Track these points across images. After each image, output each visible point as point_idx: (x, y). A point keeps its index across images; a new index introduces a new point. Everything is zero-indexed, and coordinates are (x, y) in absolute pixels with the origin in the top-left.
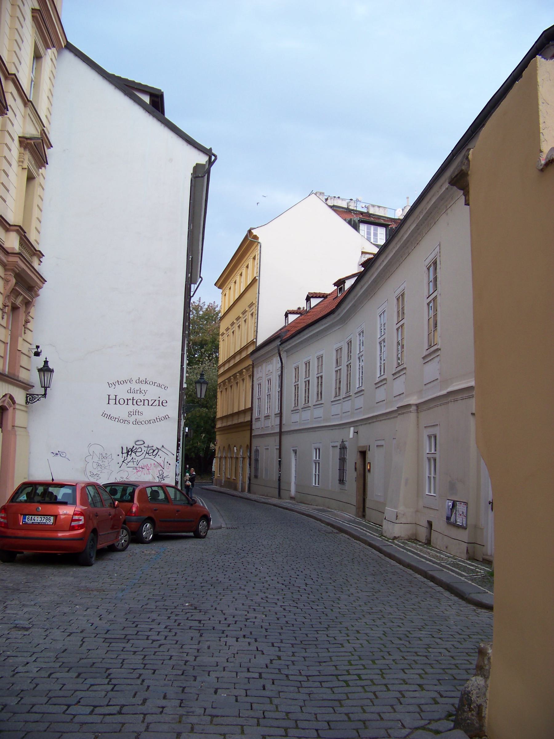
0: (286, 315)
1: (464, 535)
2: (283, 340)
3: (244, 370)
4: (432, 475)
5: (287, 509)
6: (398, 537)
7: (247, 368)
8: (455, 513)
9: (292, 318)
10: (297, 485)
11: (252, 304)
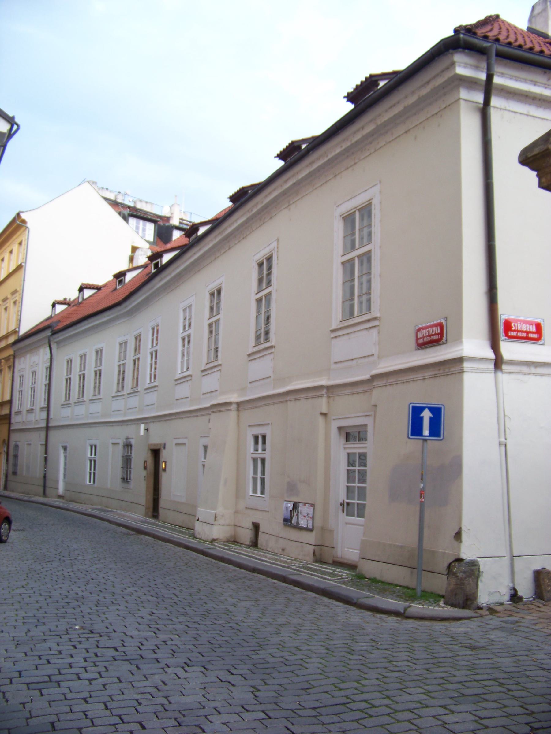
0: (54, 305)
1: (311, 538)
2: (52, 331)
3: (3, 361)
4: (259, 475)
5: (60, 508)
6: (217, 540)
7: (7, 359)
8: (297, 515)
9: (60, 308)
10: (66, 483)
11: (15, 292)
